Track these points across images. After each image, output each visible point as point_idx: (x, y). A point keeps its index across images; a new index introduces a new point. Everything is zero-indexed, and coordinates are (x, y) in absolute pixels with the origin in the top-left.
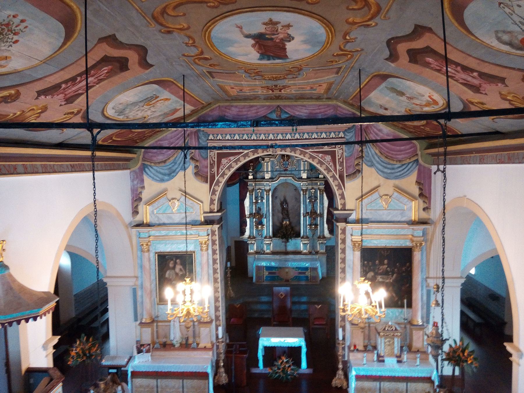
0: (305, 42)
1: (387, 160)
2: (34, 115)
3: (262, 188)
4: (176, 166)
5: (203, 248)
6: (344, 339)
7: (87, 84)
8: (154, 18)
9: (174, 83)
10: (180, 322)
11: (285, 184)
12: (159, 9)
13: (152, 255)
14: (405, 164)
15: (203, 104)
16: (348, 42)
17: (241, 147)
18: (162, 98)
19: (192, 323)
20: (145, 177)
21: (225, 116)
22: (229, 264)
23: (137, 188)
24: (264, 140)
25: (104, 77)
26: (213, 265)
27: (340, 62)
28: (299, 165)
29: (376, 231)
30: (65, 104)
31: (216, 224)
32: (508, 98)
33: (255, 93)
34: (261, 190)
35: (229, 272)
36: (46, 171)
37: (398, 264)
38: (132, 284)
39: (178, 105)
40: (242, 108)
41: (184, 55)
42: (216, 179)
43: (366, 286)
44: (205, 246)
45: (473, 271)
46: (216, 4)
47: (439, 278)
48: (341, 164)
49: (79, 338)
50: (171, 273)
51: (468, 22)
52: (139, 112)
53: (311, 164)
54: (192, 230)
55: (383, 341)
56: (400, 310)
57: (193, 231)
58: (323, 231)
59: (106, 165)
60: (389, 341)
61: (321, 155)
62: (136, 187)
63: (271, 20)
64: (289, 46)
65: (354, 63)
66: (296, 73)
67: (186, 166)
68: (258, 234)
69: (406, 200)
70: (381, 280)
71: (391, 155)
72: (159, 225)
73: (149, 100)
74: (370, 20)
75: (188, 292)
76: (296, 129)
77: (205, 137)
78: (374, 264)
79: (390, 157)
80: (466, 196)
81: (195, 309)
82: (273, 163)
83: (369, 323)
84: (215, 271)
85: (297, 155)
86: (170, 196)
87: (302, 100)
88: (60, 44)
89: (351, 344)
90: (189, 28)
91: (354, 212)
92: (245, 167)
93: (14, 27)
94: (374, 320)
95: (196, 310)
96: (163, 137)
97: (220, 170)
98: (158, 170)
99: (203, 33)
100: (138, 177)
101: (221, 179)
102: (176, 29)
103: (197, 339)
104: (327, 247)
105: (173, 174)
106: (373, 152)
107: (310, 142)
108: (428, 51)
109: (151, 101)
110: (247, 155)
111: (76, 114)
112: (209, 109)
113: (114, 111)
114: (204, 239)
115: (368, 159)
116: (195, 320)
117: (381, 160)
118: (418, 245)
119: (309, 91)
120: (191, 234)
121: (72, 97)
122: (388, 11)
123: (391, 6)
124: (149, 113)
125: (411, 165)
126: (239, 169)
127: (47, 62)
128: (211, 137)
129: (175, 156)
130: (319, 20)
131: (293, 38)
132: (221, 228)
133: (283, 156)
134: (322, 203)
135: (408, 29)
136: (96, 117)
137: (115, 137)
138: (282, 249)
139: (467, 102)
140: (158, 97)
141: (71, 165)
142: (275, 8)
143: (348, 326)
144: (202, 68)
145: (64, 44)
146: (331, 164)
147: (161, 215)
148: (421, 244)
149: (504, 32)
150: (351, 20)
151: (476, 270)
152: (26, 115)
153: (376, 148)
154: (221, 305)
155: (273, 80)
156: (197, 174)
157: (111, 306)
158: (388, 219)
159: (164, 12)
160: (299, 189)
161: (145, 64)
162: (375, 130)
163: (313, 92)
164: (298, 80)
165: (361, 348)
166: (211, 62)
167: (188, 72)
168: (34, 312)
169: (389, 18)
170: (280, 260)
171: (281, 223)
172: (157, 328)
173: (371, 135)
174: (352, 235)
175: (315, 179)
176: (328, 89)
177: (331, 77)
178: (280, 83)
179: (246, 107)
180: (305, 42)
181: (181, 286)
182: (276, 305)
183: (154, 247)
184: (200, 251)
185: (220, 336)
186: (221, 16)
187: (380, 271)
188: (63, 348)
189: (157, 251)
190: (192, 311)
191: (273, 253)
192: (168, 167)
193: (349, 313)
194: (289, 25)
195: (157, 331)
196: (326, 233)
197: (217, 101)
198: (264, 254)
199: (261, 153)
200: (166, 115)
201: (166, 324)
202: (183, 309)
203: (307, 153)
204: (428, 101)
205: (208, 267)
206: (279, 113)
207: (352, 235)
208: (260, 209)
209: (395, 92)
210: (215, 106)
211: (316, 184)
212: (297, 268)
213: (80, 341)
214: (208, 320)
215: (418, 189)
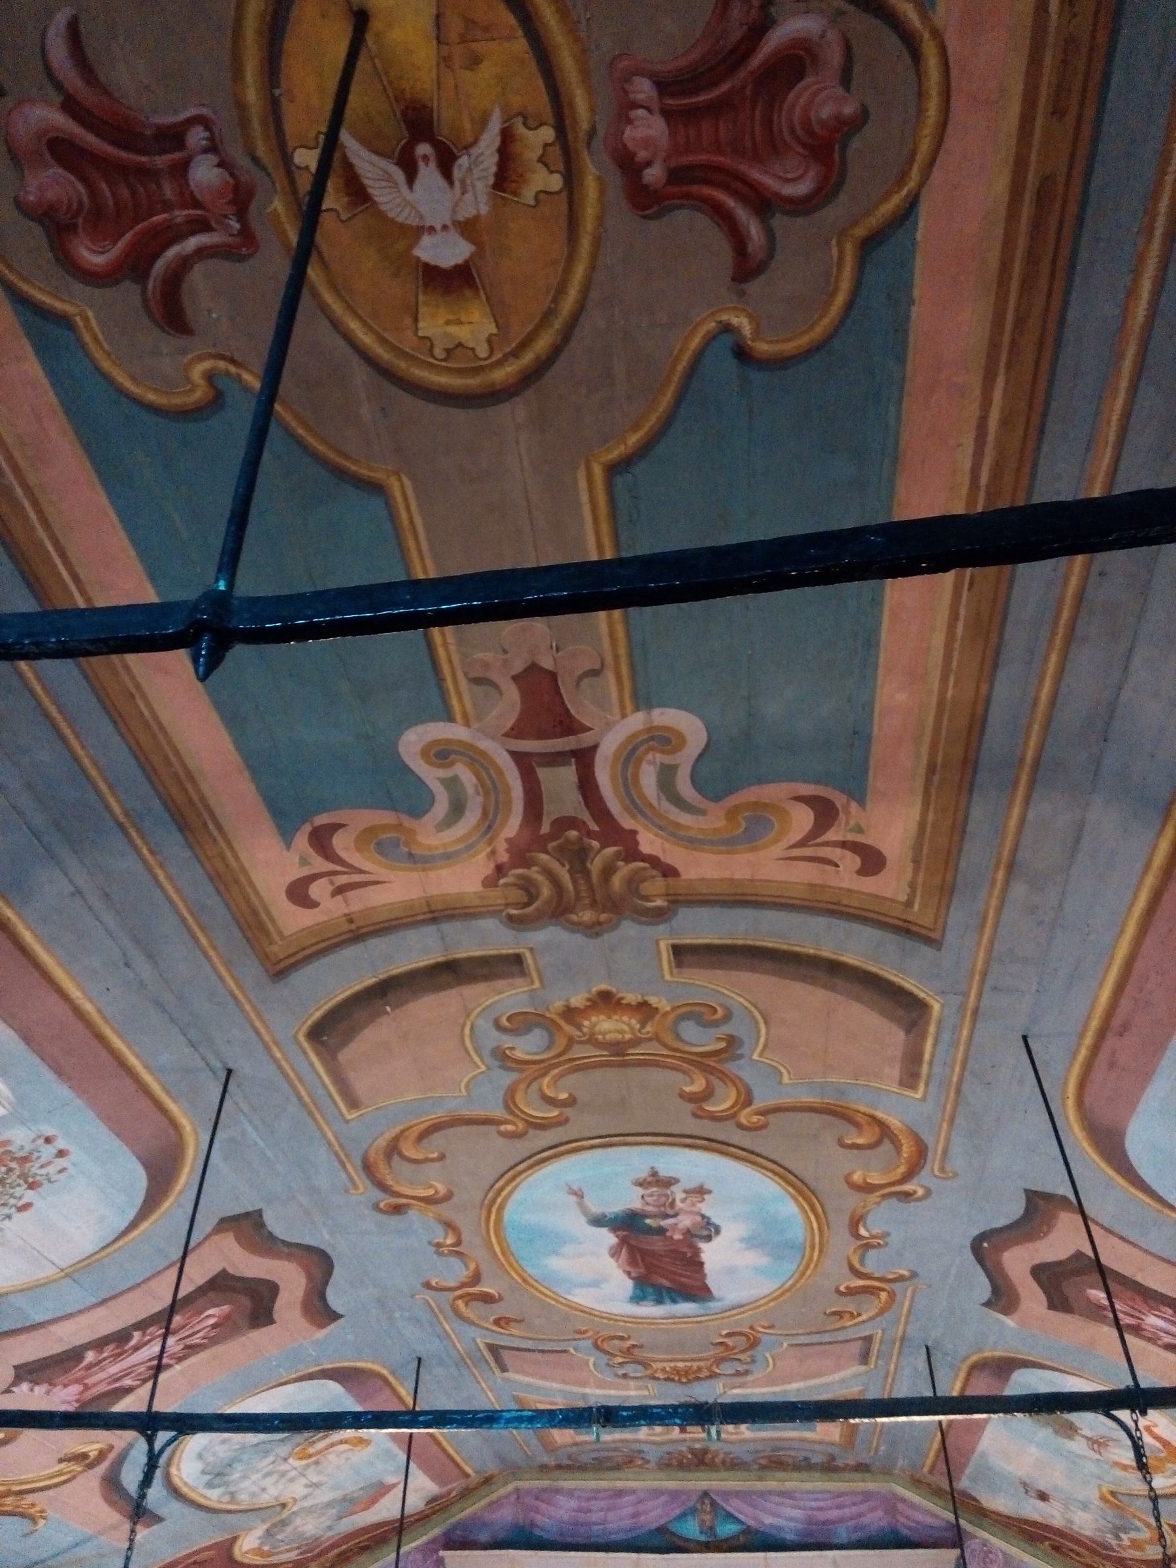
0: (752, 1242)
8: (368, 1168)
12: (382, 1142)
15: (467, 1476)
16: (867, 1247)
21: (533, 1524)
25: (204, 1338)
27: (864, 1317)
40: (589, 1499)
41: (428, 1285)
51: (1146, 1172)
52: (268, 1482)
63: (654, 1173)
64: (712, 1254)
65: (906, 1323)
66: (741, 1356)
74: (907, 1177)
76: (718, 1433)
88: (125, 1224)
99: (484, 1212)
112: (483, 1503)
113: (199, 1466)
123: (948, 1140)
127: (76, 1275)
130: (775, 1173)
142: (661, 1139)
144: (472, 1332)
145: (133, 1225)
150: (857, 1177)
155: (680, 1381)
159: (393, 1150)
164: (755, 1384)
166: (499, 1310)
167: (429, 1346)
169: (956, 1175)
179: (601, 1495)
200: (350, 1504)
210: (502, 1491)
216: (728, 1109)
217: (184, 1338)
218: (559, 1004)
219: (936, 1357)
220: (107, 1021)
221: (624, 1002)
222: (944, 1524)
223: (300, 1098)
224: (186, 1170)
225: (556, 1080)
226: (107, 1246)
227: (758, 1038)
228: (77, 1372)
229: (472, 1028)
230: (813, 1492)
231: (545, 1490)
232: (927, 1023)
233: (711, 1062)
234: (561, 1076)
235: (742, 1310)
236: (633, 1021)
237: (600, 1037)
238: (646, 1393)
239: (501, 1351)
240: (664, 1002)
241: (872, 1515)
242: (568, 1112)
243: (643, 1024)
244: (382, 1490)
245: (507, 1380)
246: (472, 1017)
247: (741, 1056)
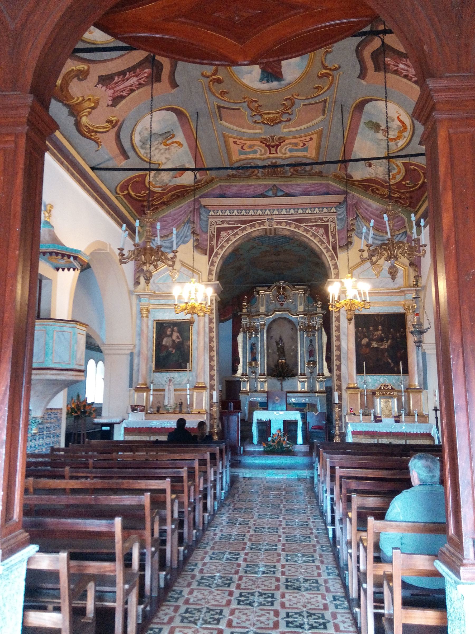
26: (210, 334)
42: (215, 250)
48: (334, 237)
50: (168, 340)
61: (314, 228)
79: (381, 230)
96: (167, 214)
97: (219, 243)
110: (244, 229)
125: (400, 236)
128: (212, 213)
134: (321, 339)
146: (324, 236)
147: (161, 284)
160: (296, 324)
162: (365, 205)
166: (222, 87)
187: (375, 337)
189: (156, 319)
196: (326, 372)
201: (161, 393)
203: (301, 226)
219: (344, 108)
231: (227, 186)
245: (222, 125)
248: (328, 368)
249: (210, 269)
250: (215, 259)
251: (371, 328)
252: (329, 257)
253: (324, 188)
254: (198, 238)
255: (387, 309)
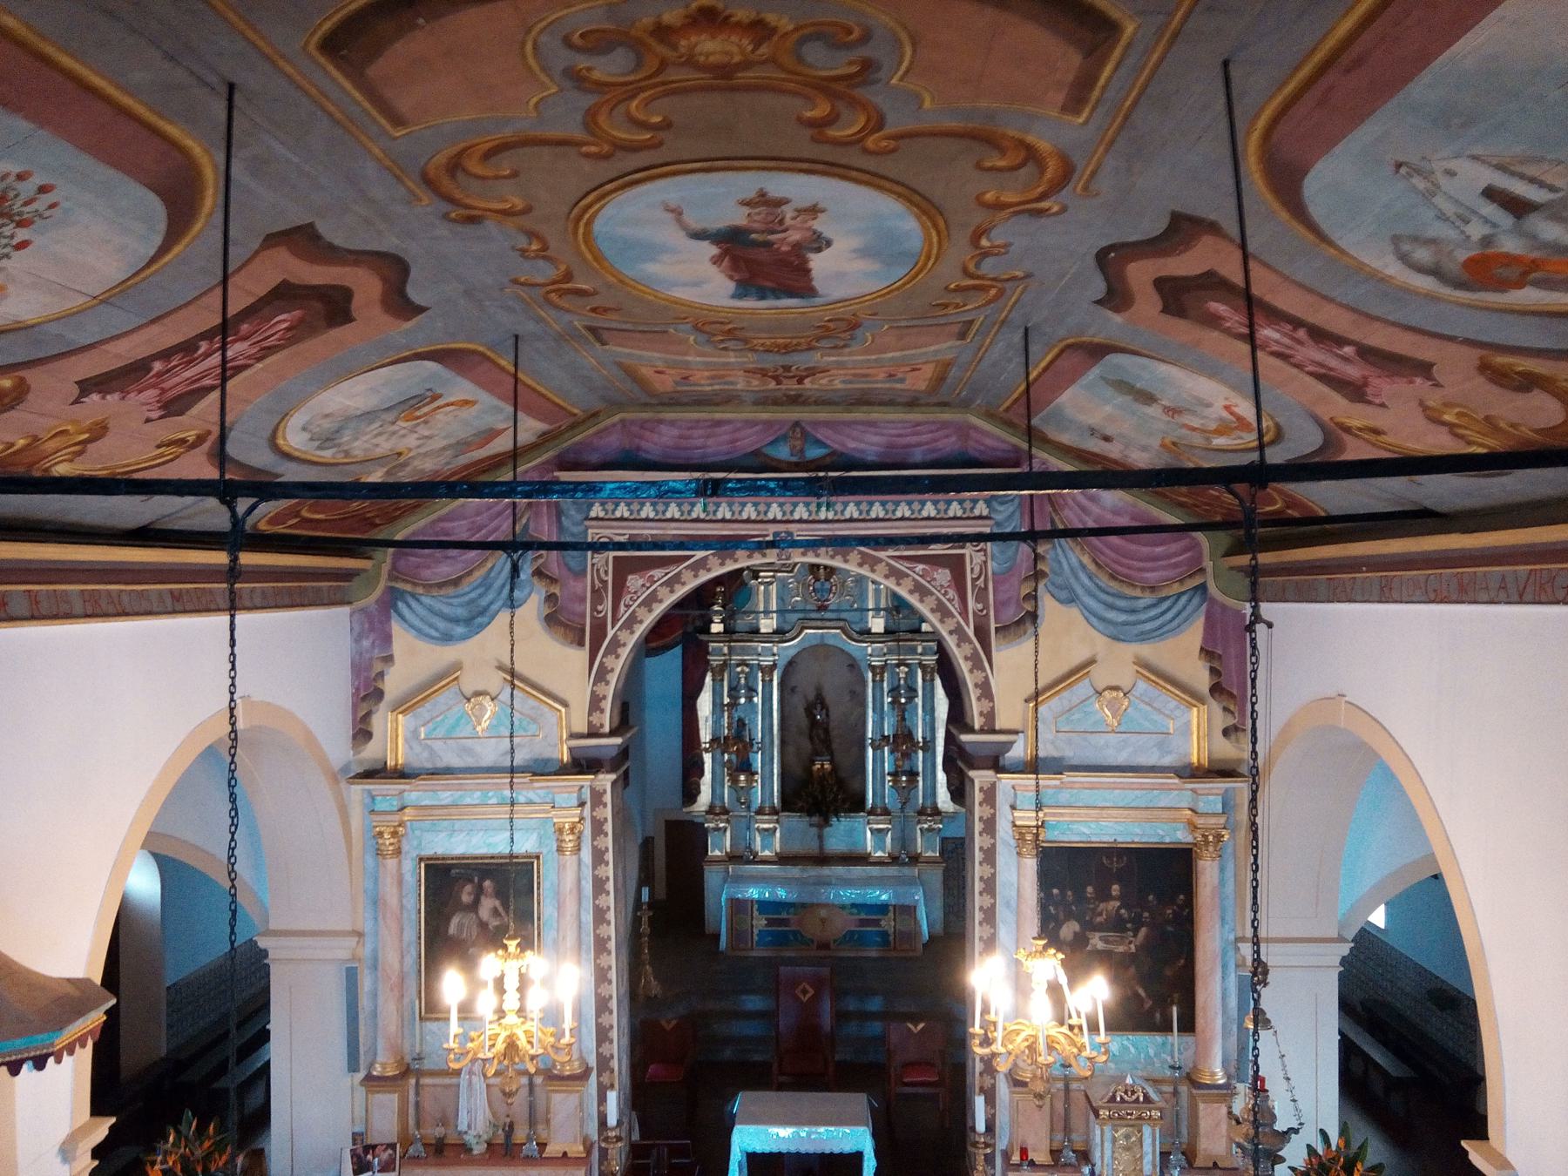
0: (864, 253)
1: (1114, 586)
2: (65, 448)
3: (751, 659)
4: (490, 596)
5: (563, 845)
6: (990, 1128)
7: (224, 361)
8: (428, 182)
9: (488, 359)
10: (485, 1076)
11: (820, 650)
12: (441, 159)
13: (409, 865)
14: (1167, 598)
15: (575, 415)
16: (986, 254)
17: (681, 545)
18: (452, 399)
19: (524, 1080)
20: (396, 628)
22: (645, 896)
23: (371, 659)
24: (755, 522)
28: (863, 596)
29: (1087, 797)
30: (161, 417)
31: (608, 772)
32: (1447, 417)
33: (726, 387)
34: (747, 665)
35: (645, 919)
36: (95, 611)
37: (1151, 897)
38: (344, 954)
39: (501, 417)
40: (691, 428)
41: (515, 282)
42: (611, 633)
43: (1048, 966)
44: (571, 837)
45: (1378, 918)
46: (606, 148)
47: (1268, 940)
48: (981, 595)
49: (176, 1123)
50: (466, 921)
51: (1316, 211)
52: (380, 440)
53: (895, 596)
54: (534, 789)
55: (1108, 1135)
56: (1158, 1038)
57: (533, 791)
58: (932, 791)
59: (277, 592)
60: (1127, 1137)
62: (368, 656)
63: (762, 194)
64: (819, 263)
65: (1010, 311)
66: (843, 335)
67: (516, 593)
68: (738, 800)
69: (1173, 704)
70: (1100, 945)
71: (1125, 571)
72: (435, 773)
73: (413, 406)
74: (1043, 197)
75: (511, 983)
77: (579, 511)
78: (1080, 897)
80: (1344, 696)
81: (531, 1036)
82: (783, 585)
83: (1067, 1081)
84: (600, 916)
85: (850, 565)
86: (469, 683)
87: (865, 408)
88: (152, 252)
89: (1011, 1144)
90: (527, 210)
91: (1020, 739)
92: (700, 598)
93: (19, 203)
94: (1081, 1069)
95: (534, 1041)
97: (622, 608)
98: (438, 606)
99: (571, 226)
100: (376, 628)
101: (623, 636)
102: (490, 210)
103: (540, 1128)
104: (944, 840)
105: (479, 620)
106: (1074, 560)
107: (892, 528)
108: (1211, 282)
109: (419, 408)
111: (194, 446)
112: (591, 431)
113: (307, 436)
114: (569, 817)
115: (1059, 580)
116: (532, 1070)
117: (1097, 585)
118: (1211, 838)
119: (882, 382)
120: (530, 803)
121: (180, 397)
122: (1094, 173)
124: (412, 441)
125: (1184, 599)
126: (680, 604)
129: (489, 565)
130: (900, 195)
131: (829, 243)
132: (624, 780)
133: (814, 568)
134: (930, 709)
135: (1153, 225)
136: (249, 452)
137: (309, 511)
138: (812, 847)
139: (1332, 425)
140: (440, 396)
141: (171, 592)
142: (772, 164)
143: (1003, 1090)
144: (567, 317)
145: (163, 250)
146: (952, 593)
147: (439, 743)
148: (1219, 837)
149: (1415, 239)
150: (989, 197)
151: (1388, 914)
152: (43, 447)
153: (1082, 549)
154: (616, 1020)
156: (551, 620)
157: (278, 1023)
158: (1122, 758)
159: (455, 166)
160: (863, 665)
161: (400, 305)
163: (898, 386)
164: (850, 354)
165: (1041, 1157)
167: (528, 327)
168: (38, 1042)
170: (801, 882)
171: (808, 770)
172: (417, 1094)
173: (1067, 513)
174: (1013, 808)
175: (909, 636)
176: (940, 379)
177: (946, 348)
178: (801, 361)
180: (864, 253)
181: (490, 964)
182: (786, 1021)
183: (415, 843)
184: (556, 854)
185: (612, 1120)
186: (620, 182)
187: (1099, 919)
188: (127, 1153)
190: (522, 1042)
191: (783, 859)
192: (467, 598)
193: (997, 1047)
194: (815, 206)
195: (417, 1104)
196: (943, 799)
197: (616, 405)
198: (754, 862)
199: (742, 560)
200: (464, 446)
201: (447, 1081)
202: (494, 1038)
203: (880, 560)
204: (1221, 419)
205: (580, 904)
206: (798, 443)
207: (1013, 808)
208: (741, 724)
209: (1129, 393)
210: (609, 422)
211: (913, 651)
212: (854, 905)
213: (178, 1132)
214: (576, 1068)
215: (1207, 673)
216: (852, 135)
217: (258, 342)
218: (648, 21)
219: (1033, 337)
220: (43, 37)
221: (733, 19)
222: (1010, 448)
223: (330, 115)
224: (210, 192)
225: (647, 103)
226: (143, 269)
227: (900, 63)
228: (149, 378)
229: (535, 47)
230: (893, 422)
231: (646, 421)
232: (1112, 48)
233: (840, 87)
234: (654, 98)
235: (847, 303)
236: (745, 42)
237: (702, 59)
238: (745, 360)
239: (600, 331)
240: (784, 21)
241: (946, 440)
242: (662, 135)
243: (757, 46)
244: (492, 434)
246: (534, 33)
247: (879, 81)
248: (948, 788)
249: (593, 692)
250: (609, 661)
251: (1090, 889)
252: (966, 658)
253: (953, 439)
254: (556, 590)
255: (1138, 831)
